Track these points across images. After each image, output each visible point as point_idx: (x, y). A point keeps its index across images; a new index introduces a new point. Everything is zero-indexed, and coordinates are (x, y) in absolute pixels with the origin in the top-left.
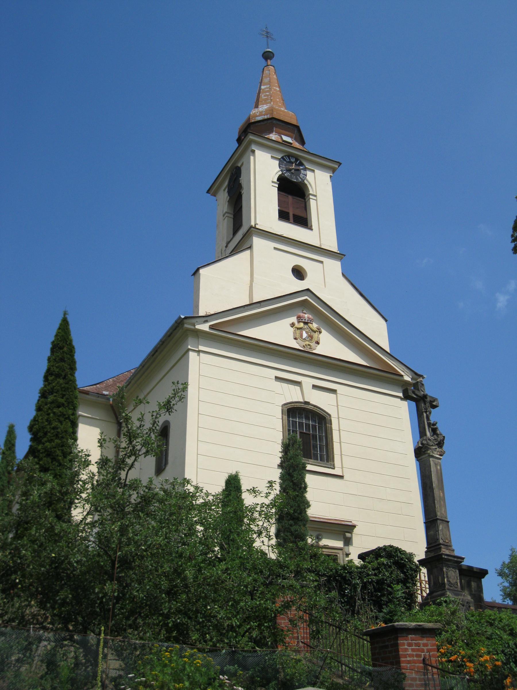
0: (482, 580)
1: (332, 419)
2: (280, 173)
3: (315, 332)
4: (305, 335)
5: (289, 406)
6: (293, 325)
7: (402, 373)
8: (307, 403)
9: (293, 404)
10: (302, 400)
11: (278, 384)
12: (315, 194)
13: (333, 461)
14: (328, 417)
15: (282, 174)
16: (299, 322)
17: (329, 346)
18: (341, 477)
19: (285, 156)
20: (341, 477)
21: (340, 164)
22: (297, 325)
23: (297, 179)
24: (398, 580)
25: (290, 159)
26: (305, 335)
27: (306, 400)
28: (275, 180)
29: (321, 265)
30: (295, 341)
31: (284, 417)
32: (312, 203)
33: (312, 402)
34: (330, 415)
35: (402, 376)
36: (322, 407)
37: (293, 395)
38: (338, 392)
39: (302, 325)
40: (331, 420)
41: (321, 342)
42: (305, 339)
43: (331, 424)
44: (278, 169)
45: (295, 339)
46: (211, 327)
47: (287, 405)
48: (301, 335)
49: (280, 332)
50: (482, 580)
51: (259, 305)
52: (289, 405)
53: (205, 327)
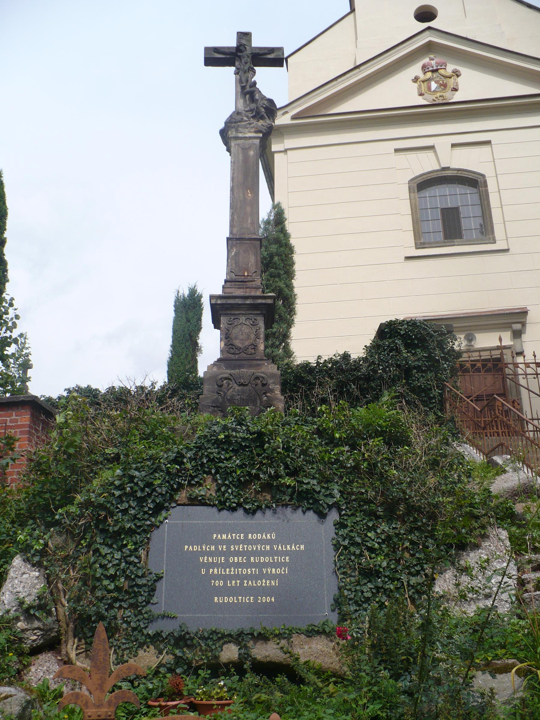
0: (357, 352)
1: (487, 179)
3: (450, 78)
4: (434, 86)
5: (420, 180)
6: (416, 80)
8: (448, 168)
9: (424, 176)
10: (437, 168)
11: (402, 156)
13: (493, 232)
14: (480, 179)
16: (425, 73)
17: (474, 85)
18: (507, 250)
20: (507, 250)
21: (520, 315)
22: (422, 77)
26: (434, 86)
27: (444, 165)
29: (486, 149)
30: (421, 97)
31: (412, 195)
33: (453, 166)
34: (483, 176)
36: (469, 169)
37: (426, 164)
38: (492, 143)
39: (429, 75)
40: (485, 182)
41: (460, 87)
43: (486, 186)
45: (421, 95)
46: (294, 118)
47: (417, 180)
48: (429, 88)
50: (357, 352)
52: (419, 178)
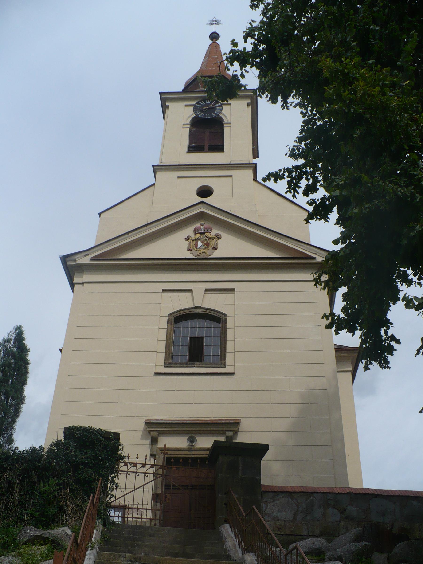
2: (194, 115)
4: (200, 244)
6: (188, 239)
7: (314, 256)
8: (199, 307)
9: (181, 312)
10: (192, 306)
11: (167, 295)
12: (229, 122)
14: (222, 318)
15: (196, 116)
17: (230, 246)
19: (201, 101)
20: (233, 374)
23: (211, 115)
24: (16, 547)
25: (205, 102)
28: (188, 122)
29: (230, 178)
32: (227, 131)
34: (225, 315)
35: (314, 258)
37: (183, 303)
42: (200, 248)
44: (192, 112)
48: (196, 246)
49: (175, 247)
51: (145, 228)
53: (86, 260)
